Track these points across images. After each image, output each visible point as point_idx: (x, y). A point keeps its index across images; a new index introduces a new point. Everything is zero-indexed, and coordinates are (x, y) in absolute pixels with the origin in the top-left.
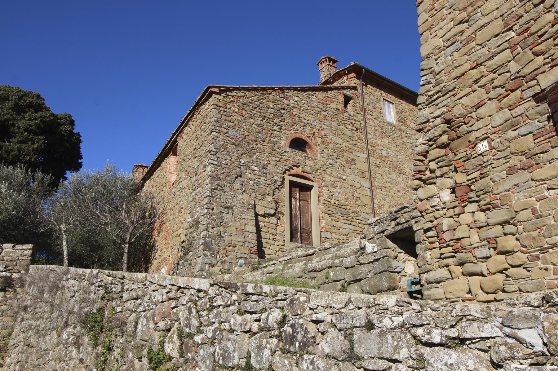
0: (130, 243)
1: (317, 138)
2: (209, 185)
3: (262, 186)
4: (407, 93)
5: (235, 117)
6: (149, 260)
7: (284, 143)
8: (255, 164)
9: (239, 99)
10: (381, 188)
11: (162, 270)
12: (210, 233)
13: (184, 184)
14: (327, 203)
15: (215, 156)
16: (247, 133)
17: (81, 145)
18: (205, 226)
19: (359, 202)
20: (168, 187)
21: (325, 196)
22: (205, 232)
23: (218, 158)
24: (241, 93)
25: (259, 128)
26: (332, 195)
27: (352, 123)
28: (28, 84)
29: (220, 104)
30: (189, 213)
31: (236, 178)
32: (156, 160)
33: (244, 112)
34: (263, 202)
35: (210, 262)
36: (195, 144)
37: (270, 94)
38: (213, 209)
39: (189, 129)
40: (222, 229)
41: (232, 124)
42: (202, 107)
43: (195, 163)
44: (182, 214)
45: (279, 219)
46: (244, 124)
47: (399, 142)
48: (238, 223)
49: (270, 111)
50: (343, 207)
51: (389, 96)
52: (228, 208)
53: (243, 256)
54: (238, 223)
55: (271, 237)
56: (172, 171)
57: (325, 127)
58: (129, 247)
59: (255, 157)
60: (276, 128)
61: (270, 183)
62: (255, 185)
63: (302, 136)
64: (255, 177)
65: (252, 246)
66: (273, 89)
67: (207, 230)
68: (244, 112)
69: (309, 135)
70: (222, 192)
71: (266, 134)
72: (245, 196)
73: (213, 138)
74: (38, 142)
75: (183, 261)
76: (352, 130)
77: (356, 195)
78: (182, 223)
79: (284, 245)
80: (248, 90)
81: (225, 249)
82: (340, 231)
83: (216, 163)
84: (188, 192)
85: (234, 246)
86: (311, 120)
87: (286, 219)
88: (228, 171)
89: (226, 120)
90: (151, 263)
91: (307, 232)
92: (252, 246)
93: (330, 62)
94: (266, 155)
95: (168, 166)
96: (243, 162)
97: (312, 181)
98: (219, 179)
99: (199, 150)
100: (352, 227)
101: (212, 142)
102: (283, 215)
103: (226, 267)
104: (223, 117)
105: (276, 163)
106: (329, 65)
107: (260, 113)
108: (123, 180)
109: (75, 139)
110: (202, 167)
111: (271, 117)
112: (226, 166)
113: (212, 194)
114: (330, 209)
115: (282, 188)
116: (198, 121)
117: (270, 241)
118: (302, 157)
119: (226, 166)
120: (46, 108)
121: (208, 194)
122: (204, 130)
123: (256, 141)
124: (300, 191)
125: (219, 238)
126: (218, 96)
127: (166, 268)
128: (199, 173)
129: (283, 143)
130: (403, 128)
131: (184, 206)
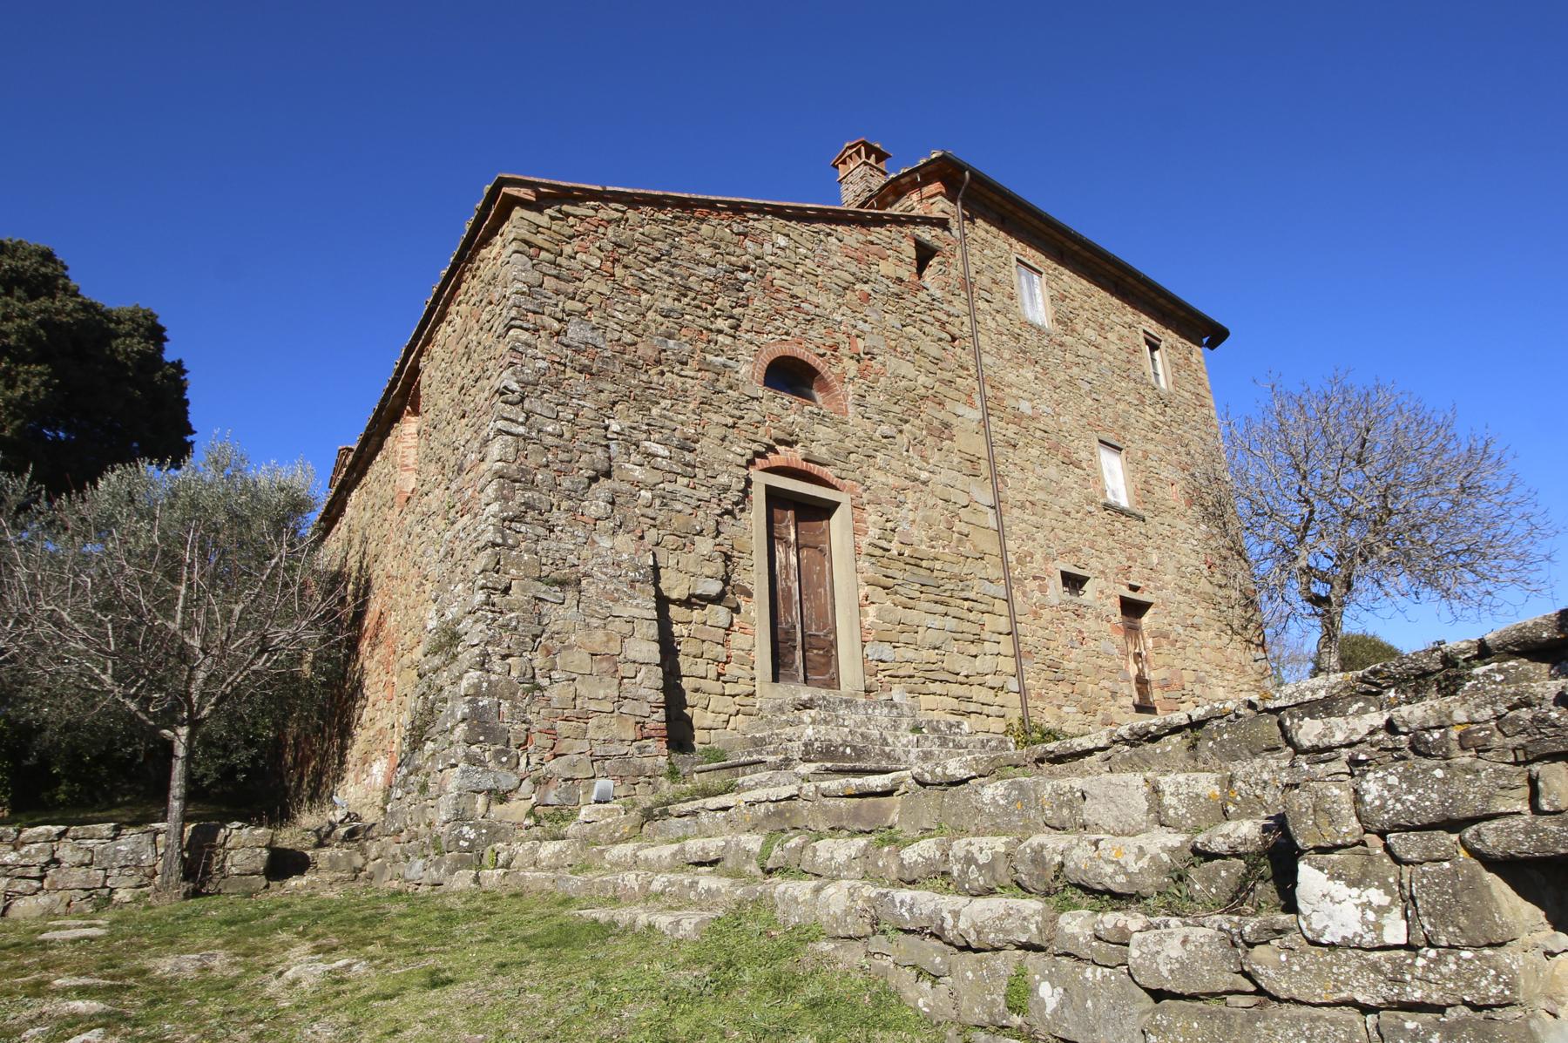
1: (845, 359)
2: (495, 507)
3: (679, 506)
4: (1076, 247)
5: (588, 285)
6: (348, 724)
7: (749, 370)
8: (657, 436)
9: (601, 230)
10: (1022, 507)
12: (493, 677)
14: (879, 553)
15: (517, 409)
16: (628, 338)
17: (189, 395)
18: (476, 651)
19: (967, 549)
21: (874, 532)
22: (474, 675)
24: (610, 212)
25: (668, 323)
26: (893, 530)
27: (938, 320)
28: (27, 229)
29: (539, 240)
32: (368, 429)
33: (619, 271)
34: (683, 558)
35: (490, 784)
37: (702, 221)
38: (506, 590)
39: (450, 329)
40: (539, 660)
41: (579, 306)
42: (483, 251)
45: (736, 610)
46: (619, 307)
47: (1061, 377)
49: (703, 271)
50: (924, 564)
51: (1030, 252)
52: (562, 584)
53: (615, 749)
54: (600, 635)
55: (713, 670)
57: (867, 327)
58: (191, 736)
59: (655, 411)
60: (721, 323)
62: (657, 502)
63: (800, 352)
64: (656, 477)
65: (646, 710)
66: (711, 205)
68: (619, 271)
69: (821, 351)
71: (691, 342)
72: (622, 540)
73: (513, 349)
74: (26, 382)
76: (940, 340)
79: (752, 694)
80: (633, 201)
81: (550, 732)
82: (919, 637)
83: (521, 430)
85: (584, 717)
86: (828, 305)
87: (756, 610)
88: (562, 456)
90: (351, 735)
91: (821, 644)
92: (646, 710)
93: (868, 157)
94: (691, 406)
95: (400, 447)
96: (615, 427)
99: (473, 391)
100: (950, 623)
101: (508, 359)
102: (749, 595)
103: (552, 798)
104: (550, 283)
105: (723, 431)
106: (865, 164)
107: (672, 275)
109: (164, 376)
110: (476, 445)
111: (706, 290)
112: (557, 441)
113: (504, 537)
114: (889, 572)
115: (742, 510)
118: (802, 415)
120: (65, 289)
121: (489, 535)
123: (658, 362)
126: (532, 216)
127: (385, 761)
129: (744, 369)
130: (1068, 340)
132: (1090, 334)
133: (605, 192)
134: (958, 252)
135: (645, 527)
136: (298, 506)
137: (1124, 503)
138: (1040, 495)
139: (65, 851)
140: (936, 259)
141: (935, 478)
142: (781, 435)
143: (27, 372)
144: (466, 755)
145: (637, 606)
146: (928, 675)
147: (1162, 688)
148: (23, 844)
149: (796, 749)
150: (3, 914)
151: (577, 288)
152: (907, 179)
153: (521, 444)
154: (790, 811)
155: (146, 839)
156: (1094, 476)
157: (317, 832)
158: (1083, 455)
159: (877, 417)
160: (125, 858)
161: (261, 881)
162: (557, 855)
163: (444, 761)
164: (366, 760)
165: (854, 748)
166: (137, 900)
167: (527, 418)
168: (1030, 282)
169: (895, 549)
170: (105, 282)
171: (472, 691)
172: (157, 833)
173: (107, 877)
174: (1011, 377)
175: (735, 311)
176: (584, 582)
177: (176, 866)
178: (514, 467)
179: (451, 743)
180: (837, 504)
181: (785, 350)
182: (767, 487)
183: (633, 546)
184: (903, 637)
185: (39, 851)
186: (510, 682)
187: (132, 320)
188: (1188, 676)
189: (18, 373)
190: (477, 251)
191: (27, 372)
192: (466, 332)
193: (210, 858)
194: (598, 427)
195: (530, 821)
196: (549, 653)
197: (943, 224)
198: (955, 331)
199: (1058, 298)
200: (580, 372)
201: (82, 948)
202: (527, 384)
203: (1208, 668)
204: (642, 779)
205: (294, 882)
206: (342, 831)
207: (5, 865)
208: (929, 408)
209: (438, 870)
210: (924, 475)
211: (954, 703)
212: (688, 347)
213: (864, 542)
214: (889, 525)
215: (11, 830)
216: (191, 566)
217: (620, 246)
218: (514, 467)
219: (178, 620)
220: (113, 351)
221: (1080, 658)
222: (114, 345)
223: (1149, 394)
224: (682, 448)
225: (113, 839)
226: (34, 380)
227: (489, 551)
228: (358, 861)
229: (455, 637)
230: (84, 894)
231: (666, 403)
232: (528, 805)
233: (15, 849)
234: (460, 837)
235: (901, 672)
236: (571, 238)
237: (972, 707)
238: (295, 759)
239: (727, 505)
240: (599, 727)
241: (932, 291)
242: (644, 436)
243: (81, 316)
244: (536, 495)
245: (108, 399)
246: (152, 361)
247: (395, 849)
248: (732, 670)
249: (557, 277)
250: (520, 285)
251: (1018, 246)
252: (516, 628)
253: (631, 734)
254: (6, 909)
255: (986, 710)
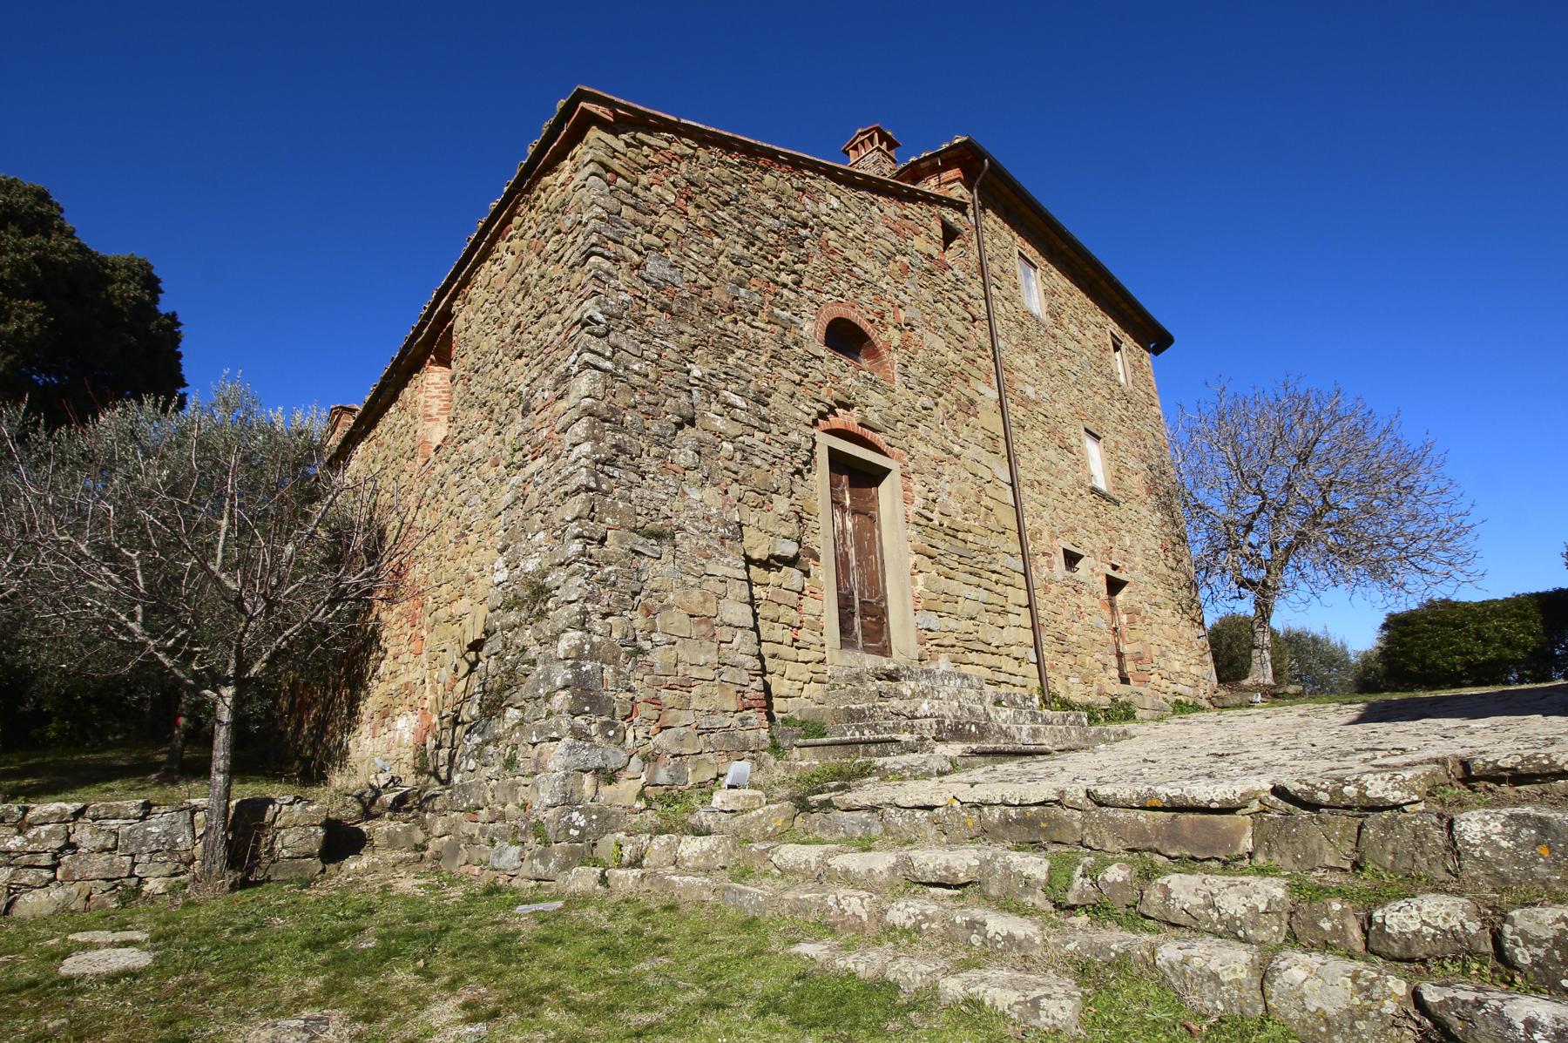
0: (241, 682)
3: (758, 462)
4: (1065, 247)
5: (664, 220)
6: (361, 676)
7: (811, 328)
8: (734, 386)
10: (1032, 486)
11: (401, 723)
12: (596, 639)
13: (477, 447)
14: (923, 521)
15: (603, 342)
16: (704, 281)
17: (183, 348)
18: (576, 608)
19: (992, 523)
20: (420, 461)
21: (919, 501)
22: (574, 636)
23: (616, 348)
24: (681, 147)
25: (739, 271)
28: (25, 167)
29: (615, 164)
30: (501, 551)
31: (680, 426)
32: (385, 378)
33: (691, 210)
35: (598, 762)
36: (518, 311)
37: (765, 171)
38: (602, 541)
39: (496, 268)
40: (640, 621)
42: (547, 180)
43: (520, 374)
44: (470, 548)
45: (807, 574)
46: (695, 248)
47: (1055, 367)
48: (696, 595)
49: (768, 221)
50: (960, 535)
51: (1028, 247)
52: (659, 536)
53: (718, 720)
54: (696, 595)
56: (434, 411)
57: (907, 299)
58: (236, 698)
59: (731, 360)
61: (781, 453)
62: (738, 455)
63: (853, 315)
64: (734, 429)
65: (745, 678)
66: (773, 155)
67: (583, 624)
68: (691, 210)
70: (633, 476)
71: (760, 292)
72: (710, 493)
73: (596, 277)
74: (20, 317)
75: (477, 739)
77: (986, 501)
78: (470, 580)
80: (704, 139)
81: (654, 701)
82: (959, 607)
83: (608, 365)
84: (492, 474)
85: (687, 685)
87: (824, 573)
88: (649, 398)
89: (635, 223)
90: (365, 687)
92: (745, 678)
94: (763, 359)
96: (696, 373)
97: (885, 454)
98: (620, 426)
99: (534, 328)
100: (983, 595)
101: (591, 287)
102: (817, 558)
103: (663, 776)
104: (627, 212)
105: (792, 388)
106: (879, 149)
108: (271, 435)
109: (159, 326)
110: (549, 382)
111: (772, 241)
112: (643, 381)
113: (597, 481)
114: (934, 542)
115: (809, 471)
116: (531, 233)
117: (783, 650)
119: (643, 381)
120: (61, 229)
121: (583, 478)
122: (555, 257)
123: (731, 309)
124: (852, 485)
125: (630, 655)
127: (414, 718)
128: (537, 403)
130: (1057, 332)
131: (479, 521)
132: (1073, 329)
133: (679, 123)
134: (974, 237)
135: (728, 481)
136: (313, 449)
137: (1101, 485)
138: (1044, 476)
139: (83, 835)
140: (957, 242)
141: (966, 453)
142: (842, 398)
143: (21, 307)
144: (572, 729)
145: (728, 565)
146: (967, 645)
147: (1136, 660)
148: (31, 825)
149: (928, 727)
150: (7, 912)
151: (654, 222)
152: (927, 163)
153: (609, 381)
154: (1049, 820)
155: (182, 818)
156: (1081, 463)
157: (359, 798)
158: (1074, 441)
159: (918, 388)
160: (157, 841)
161: (316, 865)
162: (707, 855)
163: (541, 731)
164: (386, 713)
165: (977, 725)
166: (171, 890)
167: (614, 353)
168: (1027, 275)
169: (936, 516)
170: (104, 228)
171: (573, 654)
172: (194, 810)
173: (134, 864)
174: (1018, 362)
175: (797, 267)
176: (678, 536)
177: (220, 851)
178: (603, 404)
179: (550, 714)
180: (889, 471)
181: (841, 311)
182: (830, 449)
183: (720, 500)
184: (946, 607)
185: (50, 834)
186: (612, 644)
187: (127, 267)
188: (1155, 650)
189: (12, 308)
190: (538, 179)
191: (21, 307)
192: (520, 268)
193: (258, 840)
194: (681, 370)
195: (640, 805)
196: (649, 613)
197: (960, 207)
198: (975, 313)
199: (1051, 293)
200: (661, 310)
201: (125, 993)
202: (612, 316)
203: (1167, 643)
204: (746, 754)
205: (352, 864)
206: (389, 798)
207: (8, 852)
208: (957, 382)
209: (545, 863)
210: (957, 449)
211: (987, 673)
212: (757, 298)
213: (913, 509)
214: (931, 495)
215: (15, 808)
216: (232, 498)
217: (693, 184)
218: (603, 404)
219: (219, 560)
220: (110, 296)
221: (1080, 631)
222: (110, 289)
223: (1117, 390)
224: (758, 402)
225: (142, 819)
226: (27, 316)
227: (583, 495)
228: (419, 836)
229: (540, 592)
230: (106, 886)
231: (740, 353)
232: (637, 785)
233: (20, 832)
234: (570, 824)
235: (946, 642)
236: (646, 167)
237: (1003, 677)
238: (292, 704)
239: (798, 463)
240: (703, 697)
241: (956, 271)
242: (723, 385)
243: (77, 257)
244: (627, 438)
245: (105, 344)
246: (146, 310)
247: (468, 828)
248: (804, 635)
249: (634, 207)
250: (600, 210)
251: (1019, 240)
252: (614, 584)
253: (732, 704)
254: (10, 905)
255: (1013, 680)
